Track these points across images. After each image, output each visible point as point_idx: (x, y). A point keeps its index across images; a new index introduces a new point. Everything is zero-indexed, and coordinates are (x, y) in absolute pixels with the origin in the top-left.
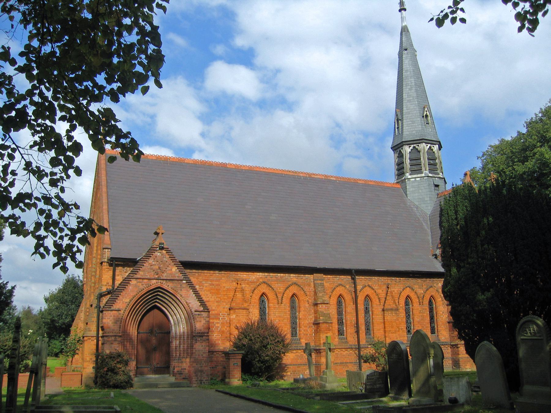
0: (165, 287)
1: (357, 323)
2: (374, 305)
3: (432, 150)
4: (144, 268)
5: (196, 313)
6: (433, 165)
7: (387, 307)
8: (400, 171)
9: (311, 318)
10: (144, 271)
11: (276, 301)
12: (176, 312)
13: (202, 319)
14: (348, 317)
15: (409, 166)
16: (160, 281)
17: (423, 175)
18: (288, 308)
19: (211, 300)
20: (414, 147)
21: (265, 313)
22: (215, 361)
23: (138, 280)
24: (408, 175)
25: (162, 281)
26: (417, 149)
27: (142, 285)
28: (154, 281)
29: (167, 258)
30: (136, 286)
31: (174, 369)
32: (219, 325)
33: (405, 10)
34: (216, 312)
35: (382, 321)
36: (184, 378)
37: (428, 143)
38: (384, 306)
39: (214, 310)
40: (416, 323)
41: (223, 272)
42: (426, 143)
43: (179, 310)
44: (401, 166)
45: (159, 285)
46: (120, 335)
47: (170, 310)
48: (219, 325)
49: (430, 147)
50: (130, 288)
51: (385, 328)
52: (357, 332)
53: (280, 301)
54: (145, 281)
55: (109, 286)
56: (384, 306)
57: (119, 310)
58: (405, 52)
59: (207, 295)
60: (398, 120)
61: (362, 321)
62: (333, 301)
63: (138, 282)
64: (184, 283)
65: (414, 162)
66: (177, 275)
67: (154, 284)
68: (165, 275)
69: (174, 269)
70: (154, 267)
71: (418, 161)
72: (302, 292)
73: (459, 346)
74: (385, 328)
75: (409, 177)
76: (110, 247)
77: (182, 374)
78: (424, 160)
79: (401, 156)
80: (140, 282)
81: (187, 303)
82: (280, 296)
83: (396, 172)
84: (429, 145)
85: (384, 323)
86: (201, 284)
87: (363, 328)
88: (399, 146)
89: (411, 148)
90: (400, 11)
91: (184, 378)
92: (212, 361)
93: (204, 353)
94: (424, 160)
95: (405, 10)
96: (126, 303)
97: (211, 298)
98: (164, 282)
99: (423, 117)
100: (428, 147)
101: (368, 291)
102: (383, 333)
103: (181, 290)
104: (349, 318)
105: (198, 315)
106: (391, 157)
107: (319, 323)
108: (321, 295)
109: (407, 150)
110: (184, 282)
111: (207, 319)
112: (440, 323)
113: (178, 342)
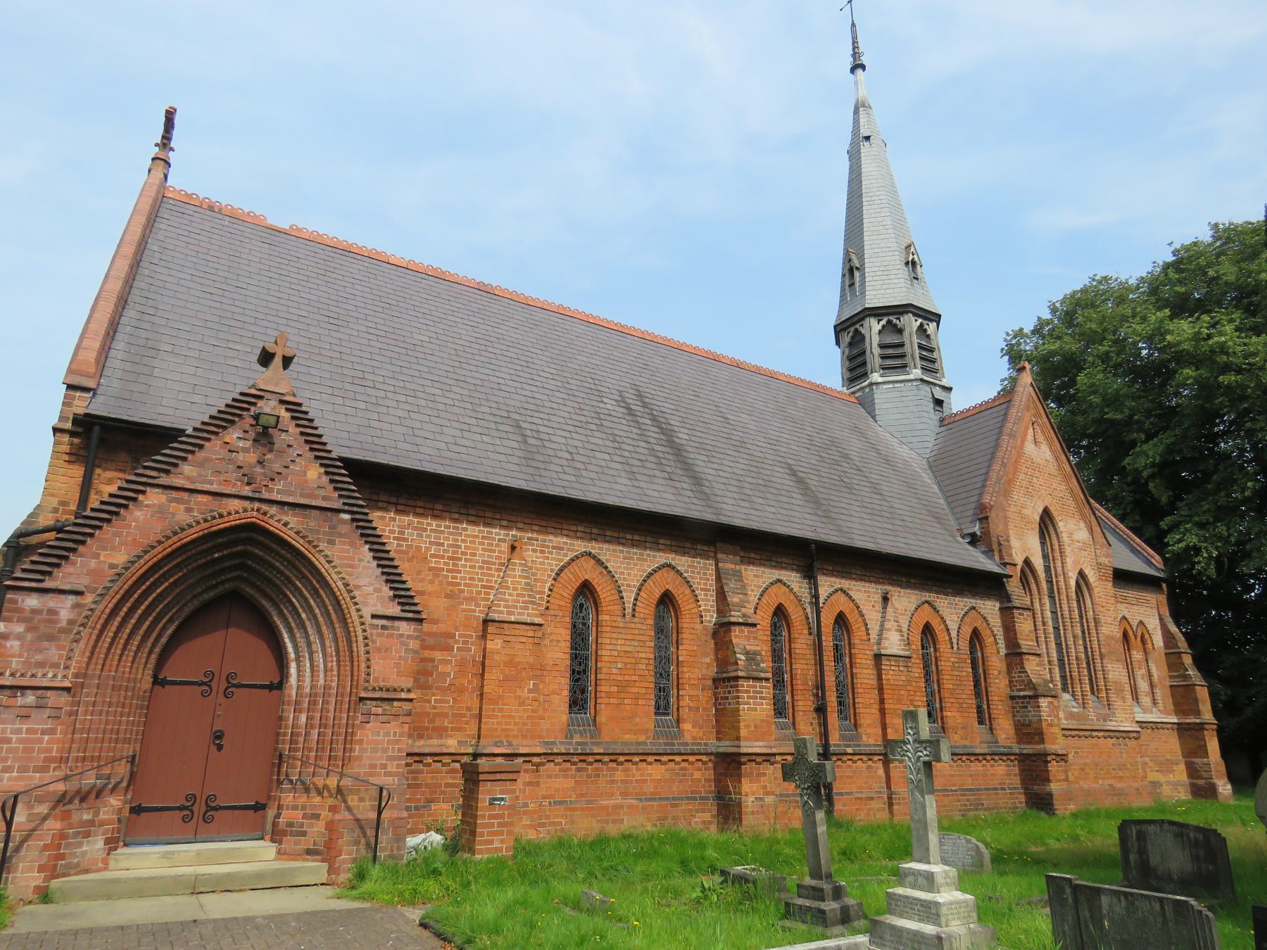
0: (274, 526)
2: (856, 641)
3: (925, 331)
4: (201, 455)
5: (376, 622)
6: (930, 360)
8: (856, 368)
10: (201, 465)
11: (617, 609)
12: (317, 646)
14: (799, 667)
16: (256, 505)
17: (911, 377)
19: (430, 588)
20: (889, 322)
21: (585, 640)
22: (427, 786)
23: (174, 494)
24: (876, 377)
25: (265, 507)
26: (895, 325)
27: (189, 510)
28: (235, 504)
30: (161, 511)
31: (278, 816)
32: (448, 669)
33: (863, 67)
34: (442, 627)
35: (875, 682)
36: (309, 852)
37: (919, 316)
39: (436, 622)
40: (945, 694)
42: (915, 315)
44: (860, 360)
45: (252, 517)
46: (67, 684)
47: (302, 642)
48: (448, 669)
49: (921, 325)
51: (882, 701)
52: (821, 710)
53: (629, 610)
54: (200, 498)
55: (65, 512)
58: (867, 144)
59: (419, 572)
60: (851, 271)
62: (764, 620)
63: (171, 500)
64: (344, 521)
66: (322, 492)
67: (236, 512)
68: (279, 486)
70: (240, 458)
71: (899, 351)
72: (688, 591)
73: (1049, 758)
74: (882, 701)
75: (880, 380)
76: (92, 384)
77: (304, 834)
79: (858, 339)
80: (179, 501)
81: (346, 585)
82: (629, 597)
83: (848, 375)
84: (920, 320)
85: (881, 689)
87: (832, 699)
88: (855, 320)
89: (883, 322)
90: (853, 70)
91: (309, 852)
92: (418, 786)
93: (390, 758)
95: (863, 67)
96: (112, 566)
97: (431, 582)
98: (273, 510)
99: (907, 263)
100: (918, 323)
101: (841, 603)
102: (878, 716)
103: (331, 542)
104: (803, 669)
105: (384, 627)
107: (737, 678)
108: (736, 600)
109: (873, 327)
110: (347, 517)
112: (994, 698)
113: (303, 718)
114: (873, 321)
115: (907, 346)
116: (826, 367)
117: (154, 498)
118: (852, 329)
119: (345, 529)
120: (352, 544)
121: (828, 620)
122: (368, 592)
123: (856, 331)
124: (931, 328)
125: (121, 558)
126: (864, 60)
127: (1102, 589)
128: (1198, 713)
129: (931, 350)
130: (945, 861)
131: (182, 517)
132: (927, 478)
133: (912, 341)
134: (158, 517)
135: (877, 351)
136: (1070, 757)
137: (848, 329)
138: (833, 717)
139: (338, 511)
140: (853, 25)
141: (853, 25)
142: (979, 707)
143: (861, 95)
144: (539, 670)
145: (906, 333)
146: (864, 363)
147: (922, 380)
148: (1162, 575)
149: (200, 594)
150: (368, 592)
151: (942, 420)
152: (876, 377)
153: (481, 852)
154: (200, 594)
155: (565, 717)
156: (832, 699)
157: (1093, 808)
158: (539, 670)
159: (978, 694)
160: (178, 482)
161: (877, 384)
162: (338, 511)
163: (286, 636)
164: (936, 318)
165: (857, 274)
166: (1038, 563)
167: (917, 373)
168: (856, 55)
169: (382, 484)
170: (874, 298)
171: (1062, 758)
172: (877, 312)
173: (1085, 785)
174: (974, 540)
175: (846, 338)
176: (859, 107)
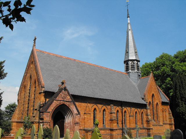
0: (65, 104)
1: (122, 120)
2: (127, 114)
7: (131, 115)
8: (127, 69)
9: (109, 118)
12: (69, 117)
13: (78, 117)
15: (130, 68)
17: (135, 71)
18: (102, 114)
24: (130, 71)
28: (62, 102)
29: (66, 93)
38: (130, 114)
41: (170, 110)
43: (71, 118)
44: (128, 67)
50: (53, 103)
52: (122, 123)
56: (130, 114)
57: (49, 112)
61: (124, 120)
65: (128, 67)
69: (69, 97)
75: (131, 71)
78: (136, 67)
79: (127, 64)
83: (125, 70)
86: (81, 107)
87: (124, 122)
94: (136, 67)
98: (65, 102)
106: (124, 66)
109: (130, 62)
111: (80, 117)
114: (130, 62)
115: (135, 66)
116: (122, 68)
117: (55, 101)
121: (123, 111)
122: (75, 112)
124: (139, 63)
125: (52, 108)
127: (160, 105)
128: (172, 122)
129: (138, 66)
131: (58, 103)
132: (137, 88)
133: (135, 65)
134: (55, 104)
135: (130, 66)
136: (153, 129)
137: (126, 62)
138: (124, 124)
139: (71, 102)
140: (128, 10)
141: (128, 10)
142: (142, 122)
144: (90, 119)
146: (128, 68)
147: (137, 72)
148: (169, 102)
149: (71, 124)
150: (75, 112)
152: (130, 71)
154: (71, 124)
155: (93, 125)
156: (124, 122)
158: (90, 119)
159: (142, 121)
160: (57, 99)
161: (131, 72)
162: (71, 102)
163: (66, 117)
164: (139, 61)
165: (128, 53)
166: (151, 102)
167: (136, 71)
169: (76, 98)
170: (130, 58)
171: (152, 129)
172: (131, 60)
173: (155, 132)
174: (143, 99)
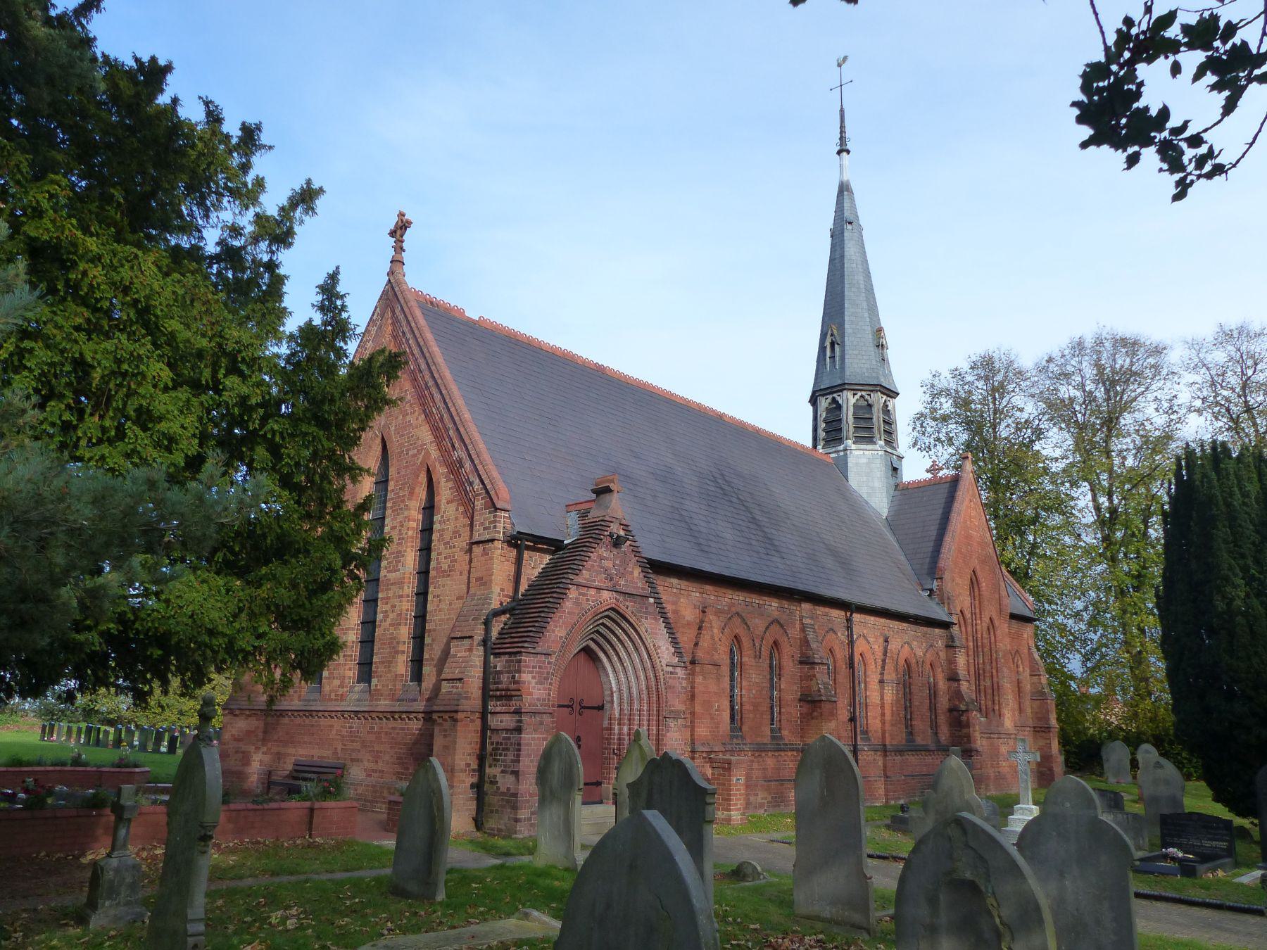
20: (862, 396)
79: (836, 407)
90: (839, 153)
114: (850, 394)
118: (830, 397)
119: (651, 609)
120: (655, 619)
123: (834, 400)
126: (849, 146)
130: (1035, 804)
140: (842, 110)
141: (842, 110)
143: (845, 179)
145: (875, 410)
151: (897, 486)
153: (162, 802)
157: (325, 673)
168: (842, 139)
175: (824, 403)
176: (844, 189)
